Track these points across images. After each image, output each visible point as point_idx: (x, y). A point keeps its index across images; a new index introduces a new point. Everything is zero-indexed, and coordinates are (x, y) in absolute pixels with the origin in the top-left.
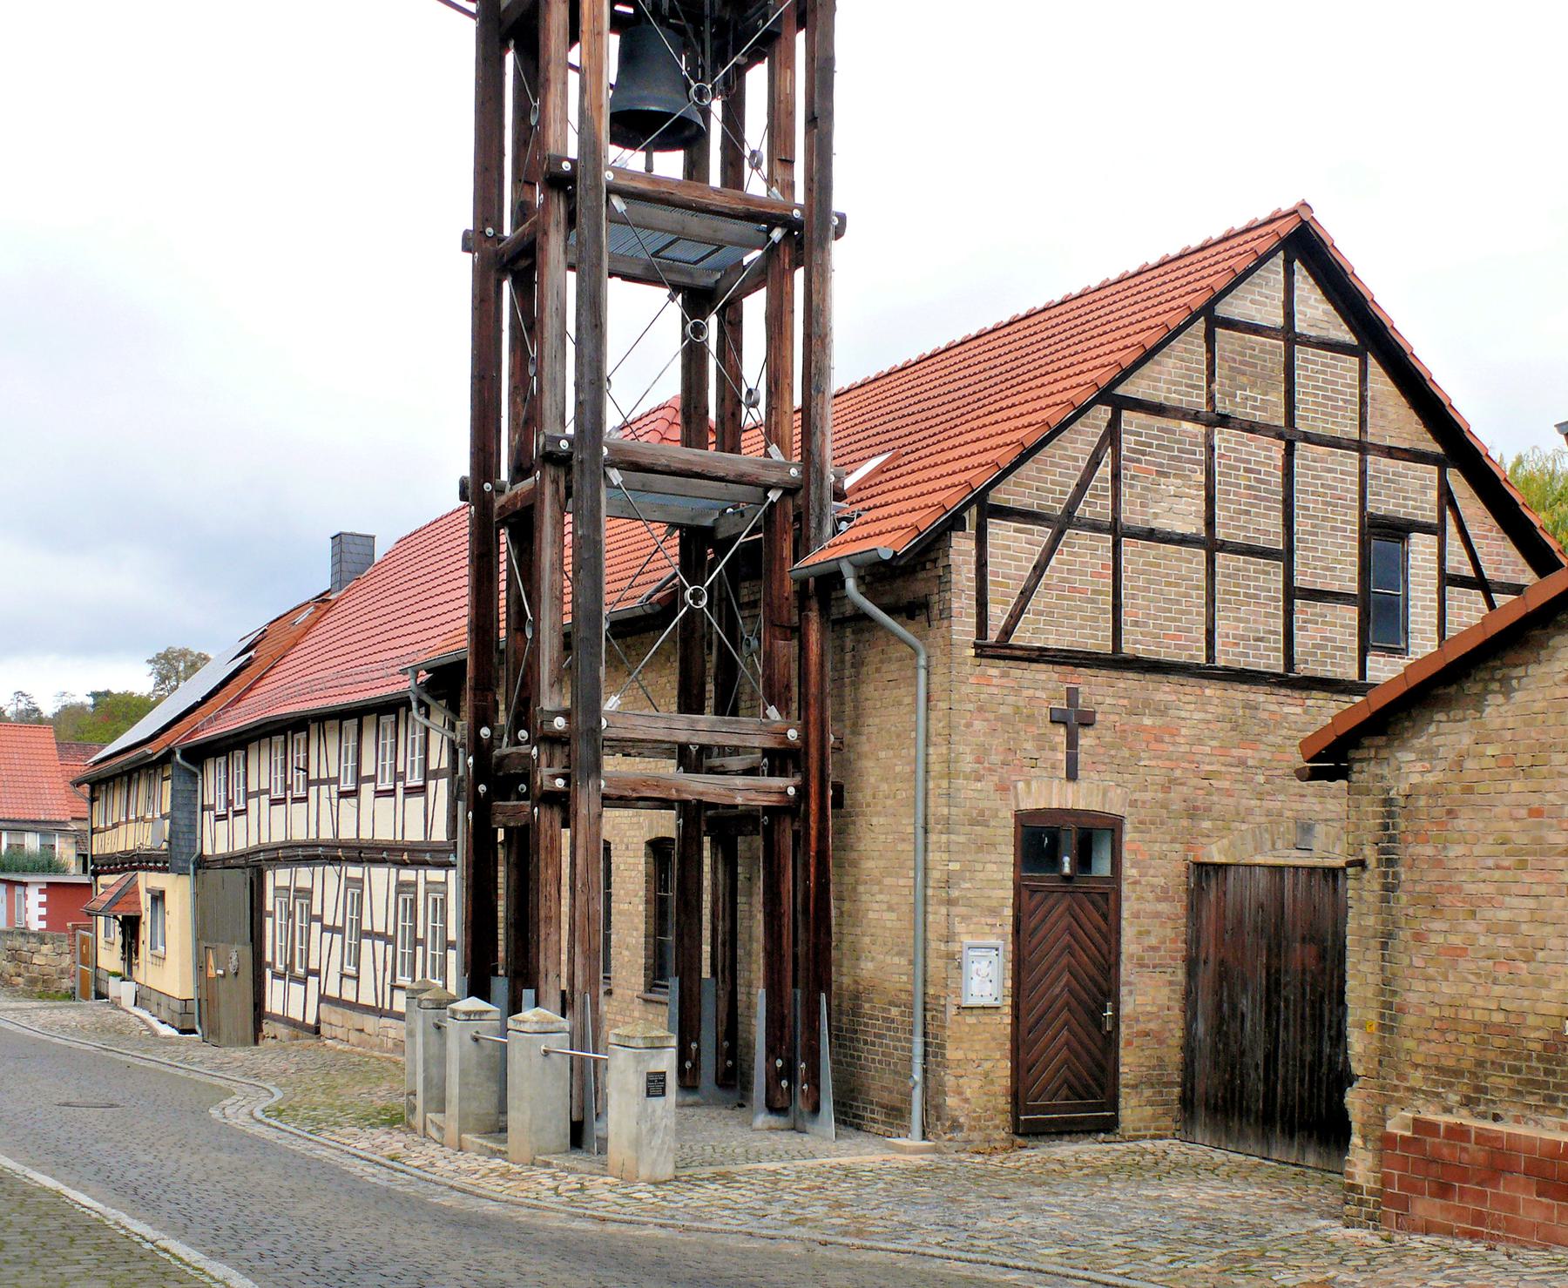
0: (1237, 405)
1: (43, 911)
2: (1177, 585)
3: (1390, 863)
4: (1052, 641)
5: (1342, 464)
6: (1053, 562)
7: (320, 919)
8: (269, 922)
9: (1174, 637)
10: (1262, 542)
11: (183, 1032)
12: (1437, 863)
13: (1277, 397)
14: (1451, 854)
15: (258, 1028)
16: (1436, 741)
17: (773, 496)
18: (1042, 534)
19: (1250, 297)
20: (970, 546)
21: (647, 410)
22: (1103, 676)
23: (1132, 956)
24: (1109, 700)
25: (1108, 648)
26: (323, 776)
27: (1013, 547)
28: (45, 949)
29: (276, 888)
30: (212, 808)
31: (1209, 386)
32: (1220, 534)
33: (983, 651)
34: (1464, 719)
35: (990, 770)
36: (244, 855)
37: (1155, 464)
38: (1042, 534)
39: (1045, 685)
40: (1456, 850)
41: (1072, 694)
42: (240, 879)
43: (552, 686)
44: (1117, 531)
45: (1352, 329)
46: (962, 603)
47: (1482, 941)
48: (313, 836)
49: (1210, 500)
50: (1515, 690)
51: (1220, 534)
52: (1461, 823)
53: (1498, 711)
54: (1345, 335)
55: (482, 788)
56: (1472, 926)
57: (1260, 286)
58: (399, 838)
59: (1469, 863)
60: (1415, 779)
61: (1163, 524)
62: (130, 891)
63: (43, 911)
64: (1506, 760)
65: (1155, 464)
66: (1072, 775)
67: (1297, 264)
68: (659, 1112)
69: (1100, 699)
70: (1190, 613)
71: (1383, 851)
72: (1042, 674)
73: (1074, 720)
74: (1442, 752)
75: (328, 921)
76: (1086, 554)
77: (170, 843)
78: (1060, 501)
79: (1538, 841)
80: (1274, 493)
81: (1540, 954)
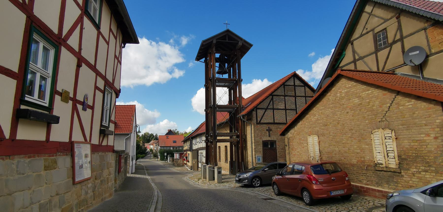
4: (266, 122)
13: (294, 93)
18: (264, 110)
21: (383, 64)
27: (260, 112)
33: (257, 123)
38: (264, 110)
39: (266, 127)
41: (269, 127)
44: (273, 109)
46: (254, 119)
49: (285, 105)
51: (287, 108)
53: (296, 128)
61: (280, 108)
62: (186, 153)
66: (269, 136)
72: (265, 125)
73: (269, 130)
76: (269, 112)
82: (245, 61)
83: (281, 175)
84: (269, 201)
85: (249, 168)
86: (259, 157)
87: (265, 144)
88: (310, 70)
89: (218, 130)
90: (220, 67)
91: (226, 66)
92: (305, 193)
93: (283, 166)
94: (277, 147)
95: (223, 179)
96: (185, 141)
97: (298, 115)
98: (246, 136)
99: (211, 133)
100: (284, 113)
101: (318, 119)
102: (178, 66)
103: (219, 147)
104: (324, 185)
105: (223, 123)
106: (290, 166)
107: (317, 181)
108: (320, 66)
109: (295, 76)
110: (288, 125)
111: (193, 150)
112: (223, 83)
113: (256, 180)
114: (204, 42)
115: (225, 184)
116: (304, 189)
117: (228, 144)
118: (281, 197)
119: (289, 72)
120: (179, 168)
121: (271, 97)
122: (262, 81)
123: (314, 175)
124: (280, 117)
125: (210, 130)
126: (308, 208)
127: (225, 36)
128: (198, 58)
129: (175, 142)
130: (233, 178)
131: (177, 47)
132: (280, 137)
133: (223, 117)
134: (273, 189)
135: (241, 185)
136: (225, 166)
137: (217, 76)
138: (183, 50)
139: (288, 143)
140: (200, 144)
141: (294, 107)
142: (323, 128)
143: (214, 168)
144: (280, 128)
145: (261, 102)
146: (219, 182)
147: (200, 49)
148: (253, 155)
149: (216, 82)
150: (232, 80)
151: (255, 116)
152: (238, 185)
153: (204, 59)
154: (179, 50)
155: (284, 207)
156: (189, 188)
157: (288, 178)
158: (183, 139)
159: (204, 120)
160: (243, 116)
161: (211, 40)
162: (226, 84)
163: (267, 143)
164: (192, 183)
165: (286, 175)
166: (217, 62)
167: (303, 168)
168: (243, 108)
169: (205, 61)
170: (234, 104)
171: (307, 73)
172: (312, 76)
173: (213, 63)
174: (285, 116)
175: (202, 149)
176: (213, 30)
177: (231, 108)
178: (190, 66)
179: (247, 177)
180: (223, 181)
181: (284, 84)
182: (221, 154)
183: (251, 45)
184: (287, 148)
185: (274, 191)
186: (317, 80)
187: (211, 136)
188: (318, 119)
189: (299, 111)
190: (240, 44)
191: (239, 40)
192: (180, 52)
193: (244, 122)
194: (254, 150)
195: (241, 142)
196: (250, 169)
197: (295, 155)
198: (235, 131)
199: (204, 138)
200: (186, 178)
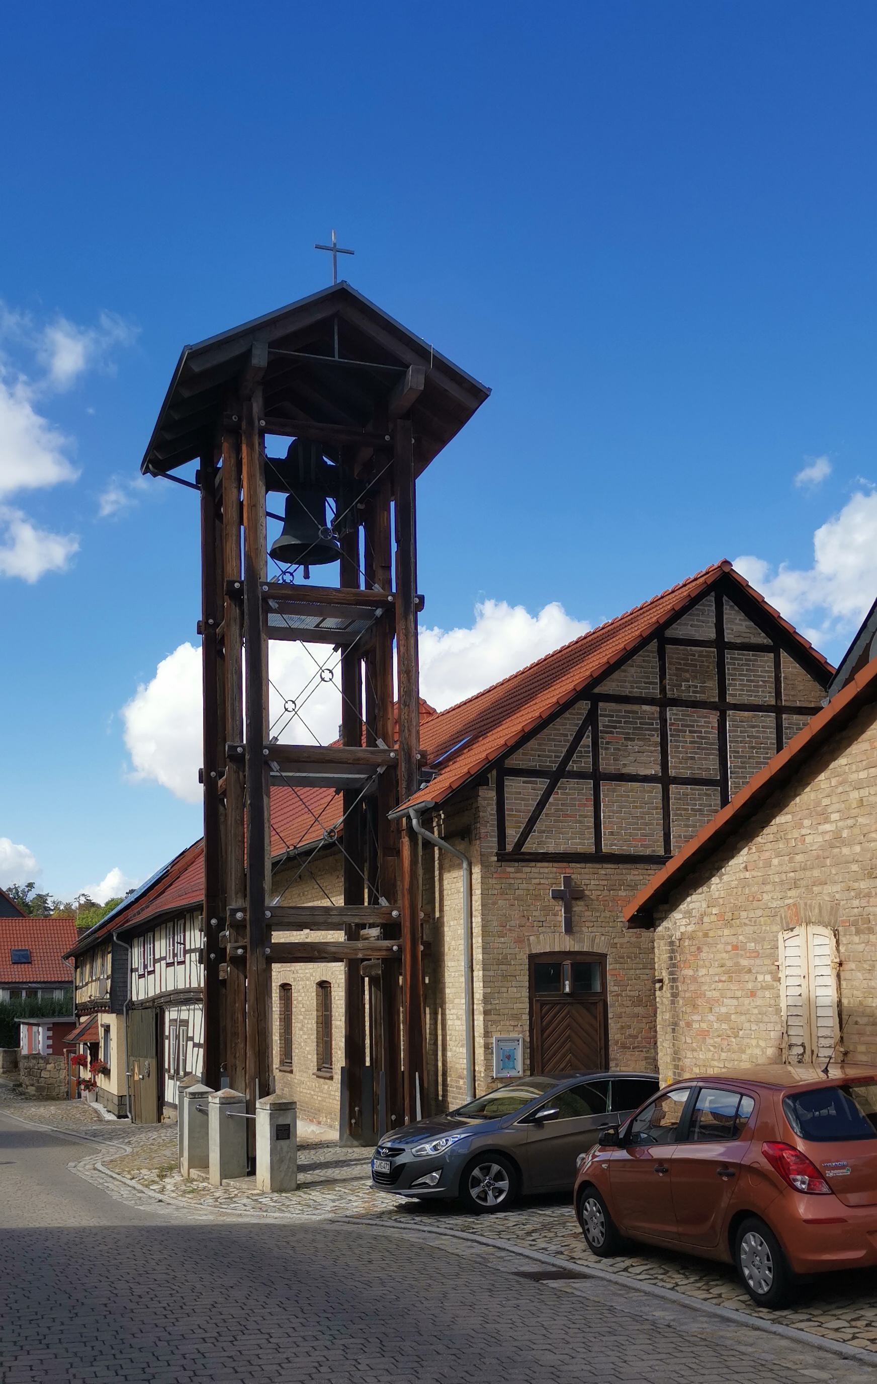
0: (683, 691)
1: (50, 1042)
2: (641, 807)
3: (674, 980)
4: (551, 847)
5: (763, 721)
6: (551, 800)
7: (192, 1039)
8: (167, 1042)
9: (640, 840)
10: (704, 775)
11: (119, 1117)
12: (694, 979)
13: (712, 684)
14: (700, 974)
15: (160, 1113)
16: (691, 906)
17: (380, 770)
18: (542, 784)
19: (691, 623)
20: (493, 794)
22: (589, 867)
23: (617, 1042)
24: (593, 882)
25: (592, 849)
26: (193, 947)
27: (521, 794)
28: (49, 1067)
29: (170, 1020)
30: (137, 970)
31: (661, 682)
32: (672, 772)
33: (503, 857)
34: (703, 893)
35: (510, 930)
36: (153, 1000)
37: (623, 733)
38: (542, 784)
39: (549, 877)
40: (702, 972)
41: (567, 880)
42: (150, 1014)
43: (236, 894)
44: (597, 777)
45: (768, 635)
46: (488, 830)
47: (716, 1025)
48: (188, 986)
50: (724, 875)
51: (672, 772)
52: (703, 955)
53: (717, 886)
54: (762, 639)
55: (212, 956)
56: (711, 1017)
57: (698, 615)
58: (188, 986)
59: (708, 979)
60: (683, 929)
61: (631, 770)
62: (93, 1025)
63: (50, 1042)
64: (720, 916)
65: (623, 733)
66: (569, 928)
67: (725, 598)
68: (285, 1149)
69: (587, 882)
70: (651, 824)
71: (671, 973)
72: (546, 868)
73: (570, 896)
74: (694, 913)
75: (196, 1040)
76: (574, 794)
77: (110, 994)
78: (555, 762)
79: (737, 964)
80: (712, 744)
81: (741, 1033)
82: (445, 491)
83: (628, 1142)
84: (553, 1284)
85: (453, 1107)
86: (507, 1047)
87: (544, 971)
88: (804, 559)
89: (277, 888)
90: (293, 517)
91: (330, 516)
92: (752, 1242)
93: (641, 1092)
94: (611, 987)
95: (303, 1168)
96: (84, 954)
97: (728, 812)
98: (437, 927)
99: (237, 905)
100: (658, 801)
101: (837, 839)
102: (42, 507)
103: (286, 988)
104: (854, 1198)
105: (308, 853)
106: (674, 1096)
107: (816, 1174)
108: (860, 538)
109: (725, 587)
110: (672, 866)
111: (132, 1006)
112: (303, 614)
113: (486, 1171)
114: (194, 354)
115: (315, 1195)
116: (744, 1220)
117: (336, 973)
118: (623, 1262)
119: (687, 567)
120: (49, 1110)
121: (584, 706)
122: (534, 612)
123: (801, 1145)
124: (630, 816)
125: (227, 890)
126: (764, 1318)
127: (324, 325)
128: (159, 461)
129: (23, 958)
130: (359, 1161)
131: (21, 390)
132: (630, 935)
133: (309, 819)
134: (582, 1222)
135: (403, 1200)
136: (318, 1101)
137: (273, 570)
138: (58, 411)
139: (673, 967)
140: (171, 969)
141: (709, 766)
142: (863, 885)
143: (250, 1108)
144: (633, 887)
145: (525, 737)
146: (279, 1187)
147: (174, 402)
148: (472, 1037)
149: (268, 610)
150: (361, 600)
151: (488, 811)
152: (388, 1200)
153: (195, 464)
154: (39, 409)
155: (636, 1318)
156: (105, 1222)
157: (661, 1161)
158: (72, 942)
159: (193, 830)
160: (426, 815)
161: (237, 350)
162: (331, 623)
163: (558, 967)
164: (125, 1192)
165: (657, 1142)
166: (272, 485)
167: (748, 1104)
168: (426, 769)
169: (206, 481)
170: (372, 743)
171: (789, 581)
172: (815, 597)
173: (253, 494)
174: (658, 815)
175: (187, 1002)
176: (250, 285)
177: (356, 764)
178: (107, 510)
179: (442, 1158)
180: (302, 1177)
181: (659, 635)
182: (296, 1026)
183: (479, 394)
184: (663, 997)
185: (586, 1232)
186: (838, 619)
187: (239, 927)
188: (837, 836)
189: (739, 798)
190: (415, 379)
191: (408, 356)
192: (39, 420)
193: (428, 845)
194: (479, 1007)
195: (407, 958)
196: (458, 1112)
197: (704, 1034)
198: (374, 901)
199: (196, 939)
200: (89, 1167)
